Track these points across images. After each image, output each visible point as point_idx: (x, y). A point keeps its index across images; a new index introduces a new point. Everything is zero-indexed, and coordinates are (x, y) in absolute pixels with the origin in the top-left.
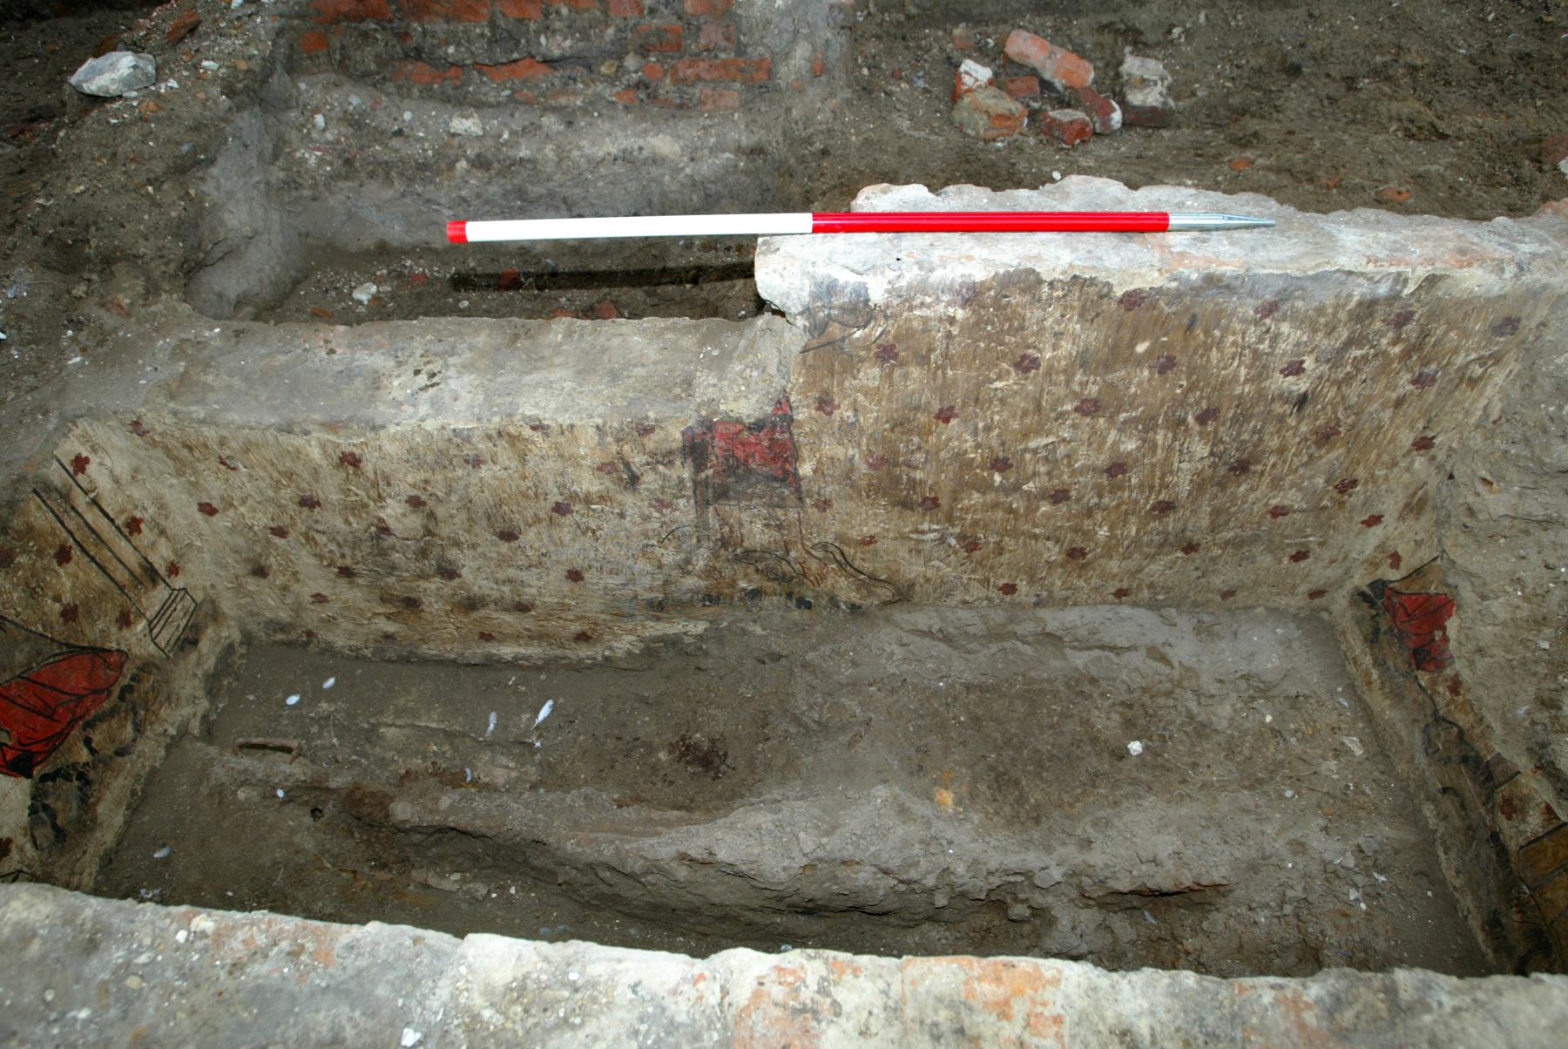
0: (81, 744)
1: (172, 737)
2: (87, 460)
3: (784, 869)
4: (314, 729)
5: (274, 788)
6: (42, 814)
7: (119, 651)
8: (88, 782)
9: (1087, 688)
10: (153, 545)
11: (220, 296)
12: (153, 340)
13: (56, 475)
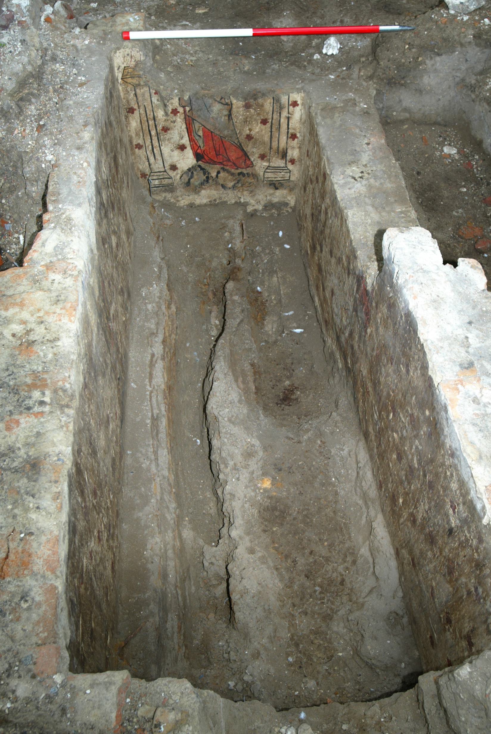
0: (216, 171)
1: (240, 202)
2: (298, 105)
3: (212, 407)
4: (267, 251)
5: (231, 243)
6: (190, 173)
7: (252, 162)
8: (207, 181)
9: (349, 559)
10: (293, 148)
11: (400, 101)
12: (351, 92)
13: (284, 99)
